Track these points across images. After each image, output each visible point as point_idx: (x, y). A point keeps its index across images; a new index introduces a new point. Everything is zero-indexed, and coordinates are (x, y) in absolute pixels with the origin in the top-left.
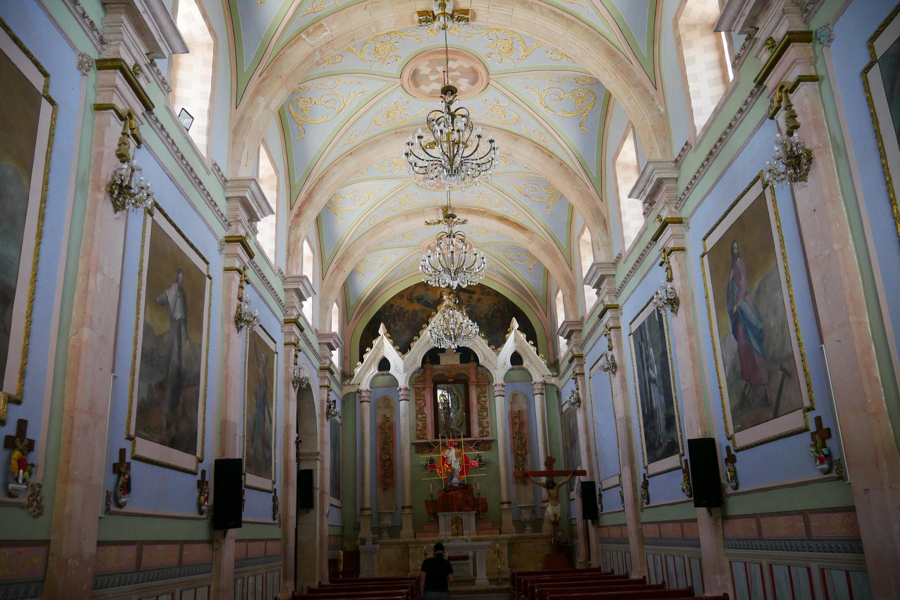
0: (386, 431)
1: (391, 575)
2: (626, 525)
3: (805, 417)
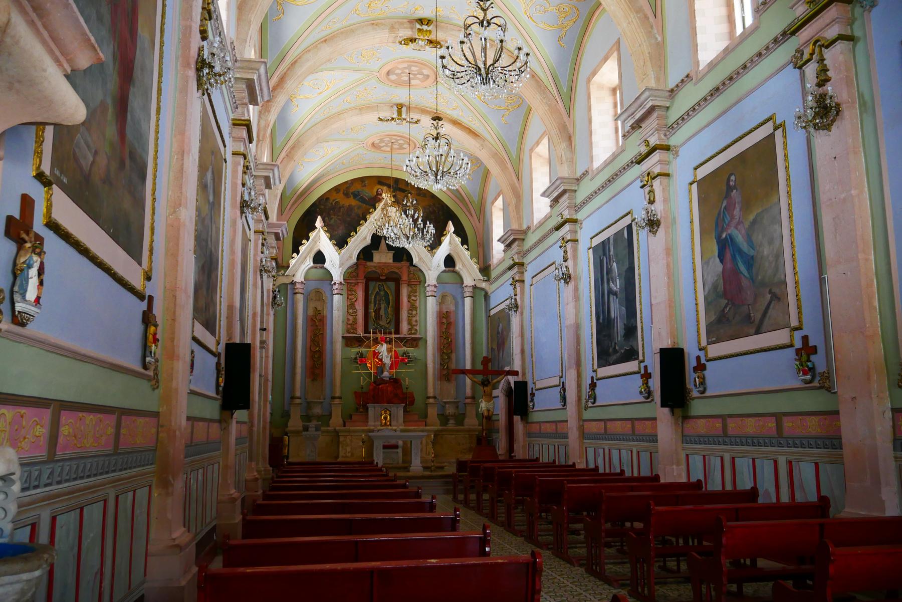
0: (317, 324)
1: (318, 460)
2: (567, 421)
3: (791, 336)
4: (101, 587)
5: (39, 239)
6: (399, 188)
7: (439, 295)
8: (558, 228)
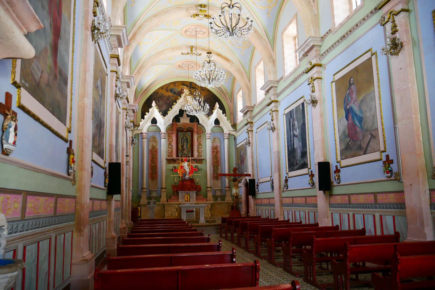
0: (154, 153)
3: (381, 155)
4: (49, 280)
5: (15, 114)
6: (192, 86)
7: (212, 138)
8: (269, 105)
